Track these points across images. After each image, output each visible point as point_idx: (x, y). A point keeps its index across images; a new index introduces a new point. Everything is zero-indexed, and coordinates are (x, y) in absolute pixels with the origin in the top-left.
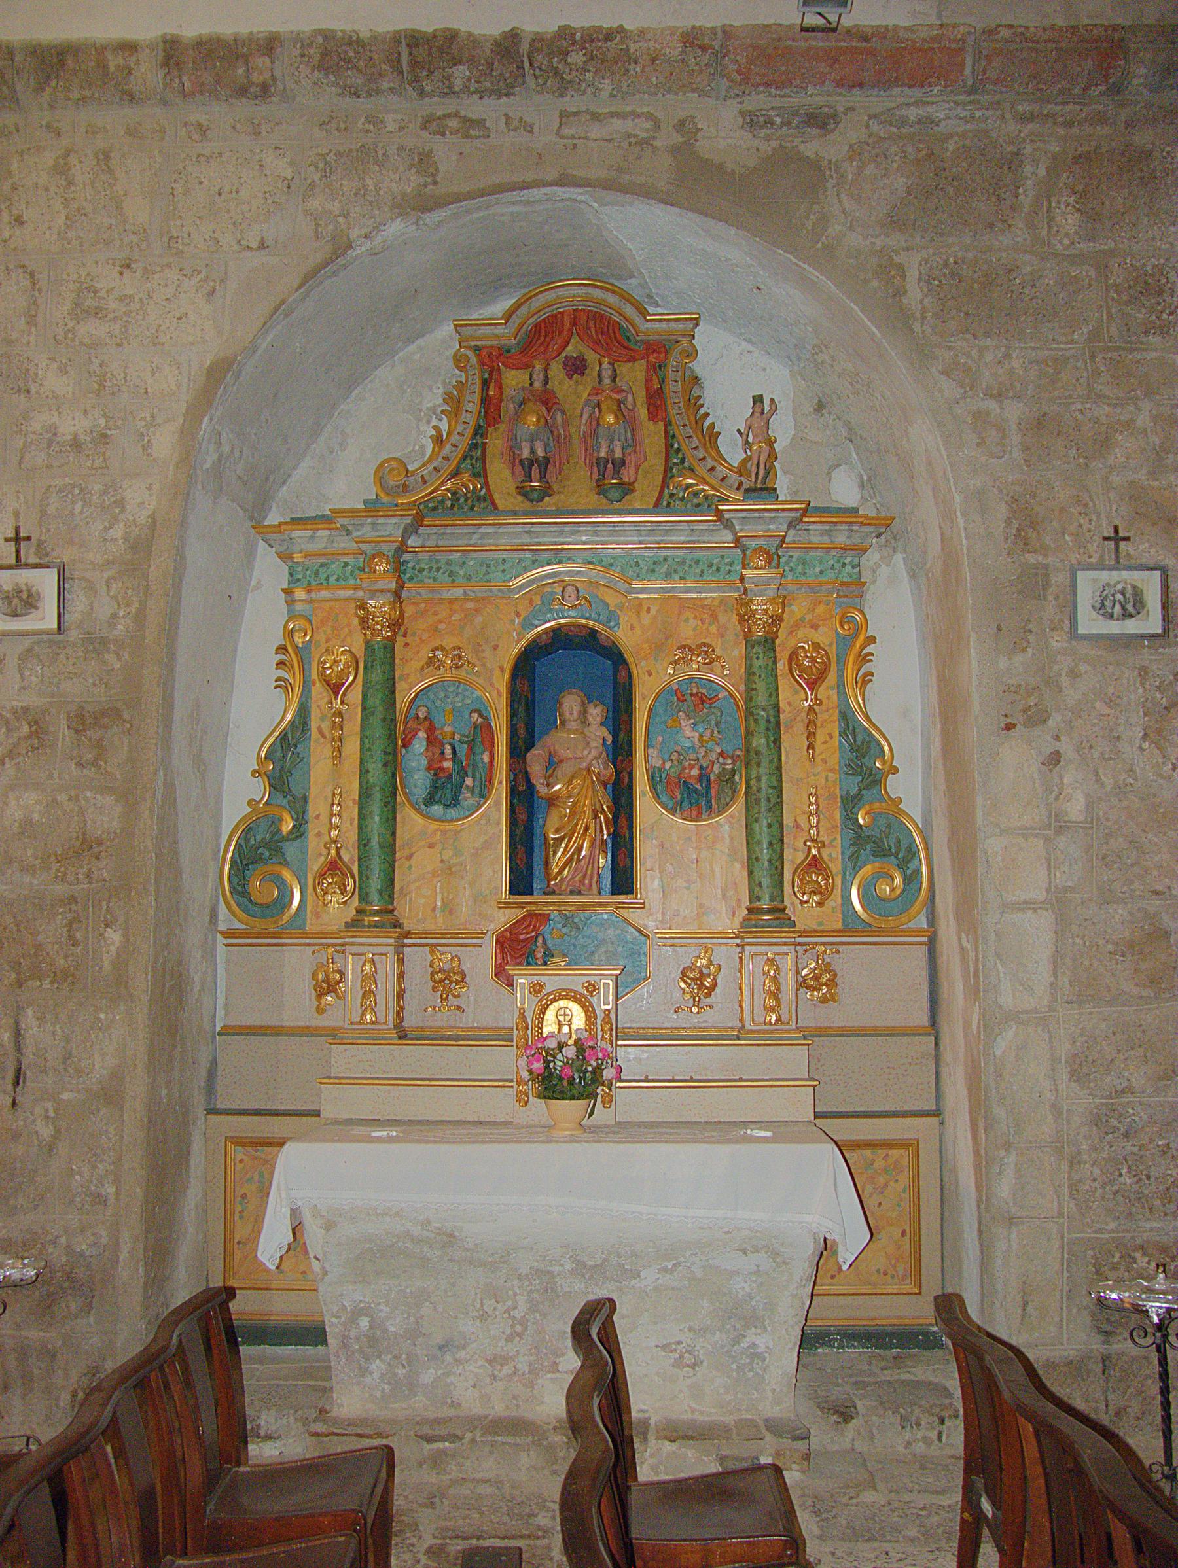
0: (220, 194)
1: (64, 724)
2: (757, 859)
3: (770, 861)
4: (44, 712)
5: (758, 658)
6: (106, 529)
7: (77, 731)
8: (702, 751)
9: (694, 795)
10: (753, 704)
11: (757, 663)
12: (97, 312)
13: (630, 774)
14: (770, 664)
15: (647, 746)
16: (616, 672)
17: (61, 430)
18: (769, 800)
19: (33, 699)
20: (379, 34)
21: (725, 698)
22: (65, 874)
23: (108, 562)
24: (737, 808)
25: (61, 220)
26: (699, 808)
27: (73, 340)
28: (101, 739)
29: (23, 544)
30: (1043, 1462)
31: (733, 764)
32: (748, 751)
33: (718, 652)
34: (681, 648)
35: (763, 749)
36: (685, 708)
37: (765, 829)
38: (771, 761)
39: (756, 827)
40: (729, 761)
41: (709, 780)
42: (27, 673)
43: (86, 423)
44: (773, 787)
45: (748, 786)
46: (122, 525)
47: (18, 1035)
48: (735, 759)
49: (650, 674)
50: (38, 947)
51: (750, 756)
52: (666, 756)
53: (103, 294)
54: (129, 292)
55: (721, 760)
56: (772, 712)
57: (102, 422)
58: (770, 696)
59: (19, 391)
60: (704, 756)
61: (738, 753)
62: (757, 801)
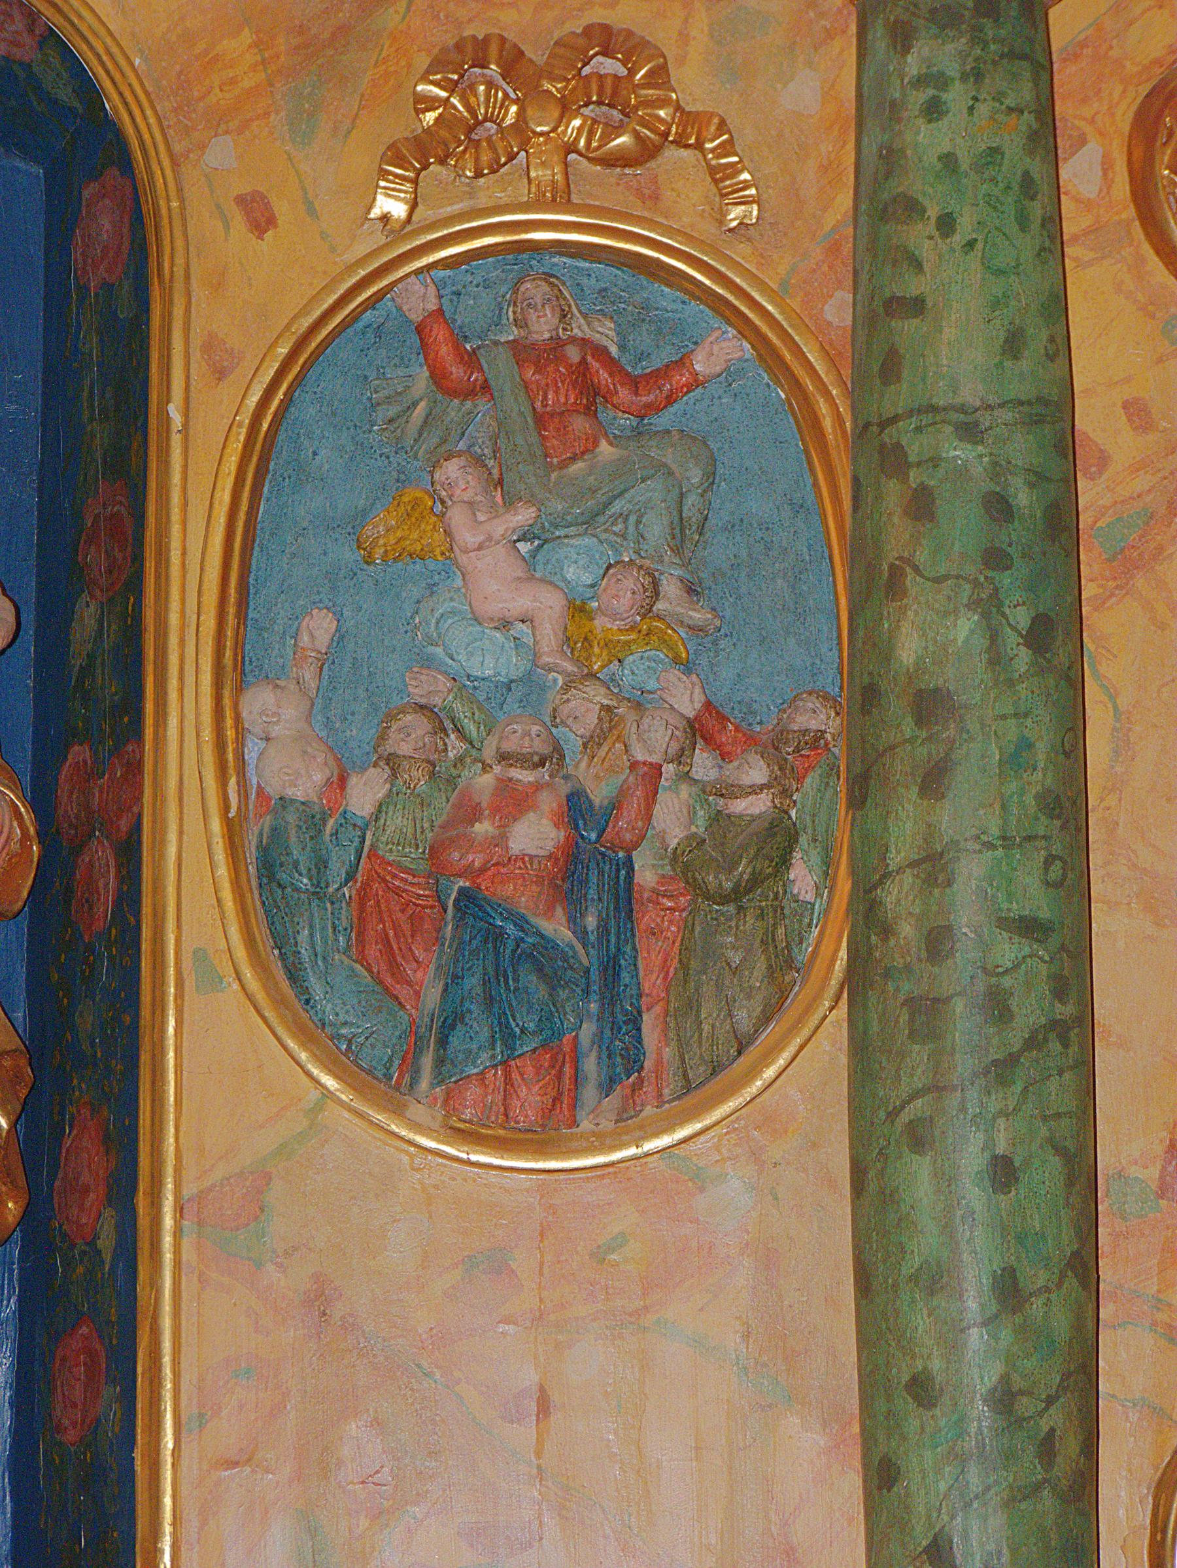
2: (922, 1389)
3: (1004, 1399)
5: (934, 110)
8: (585, 707)
9: (524, 980)
10: (899, 397)
11: (927, 140)
13: (129, 852)
14: (1013, 144)
15: (235, 672)
16: (62, 219)
18: (997, 1006)
20: (1081, 1449)
21: (730, 374)
24: (803, 1070)
26: (560, 1063)
30: (1062, 243)
31: (782, 785)
32: (869, 697)
33: (693, 86)
34: (463, 59)
35: (967, 679)
36: (480, 432)
37: (974, 1194)
38: (1017, 759)
39: (918, 1178)
40: (756, 772)
41: (624, 898)
44: (1028, 927)
45: (869, 917)
48: (791, 754)
49: (260, 218)
51: (881, 729)
52: (360, 734)
55: (704, 764)
56: (1022, 449)
58: (1013, 344)
60: (591, 743)
61: (815, 718)
62: (927, 1013)
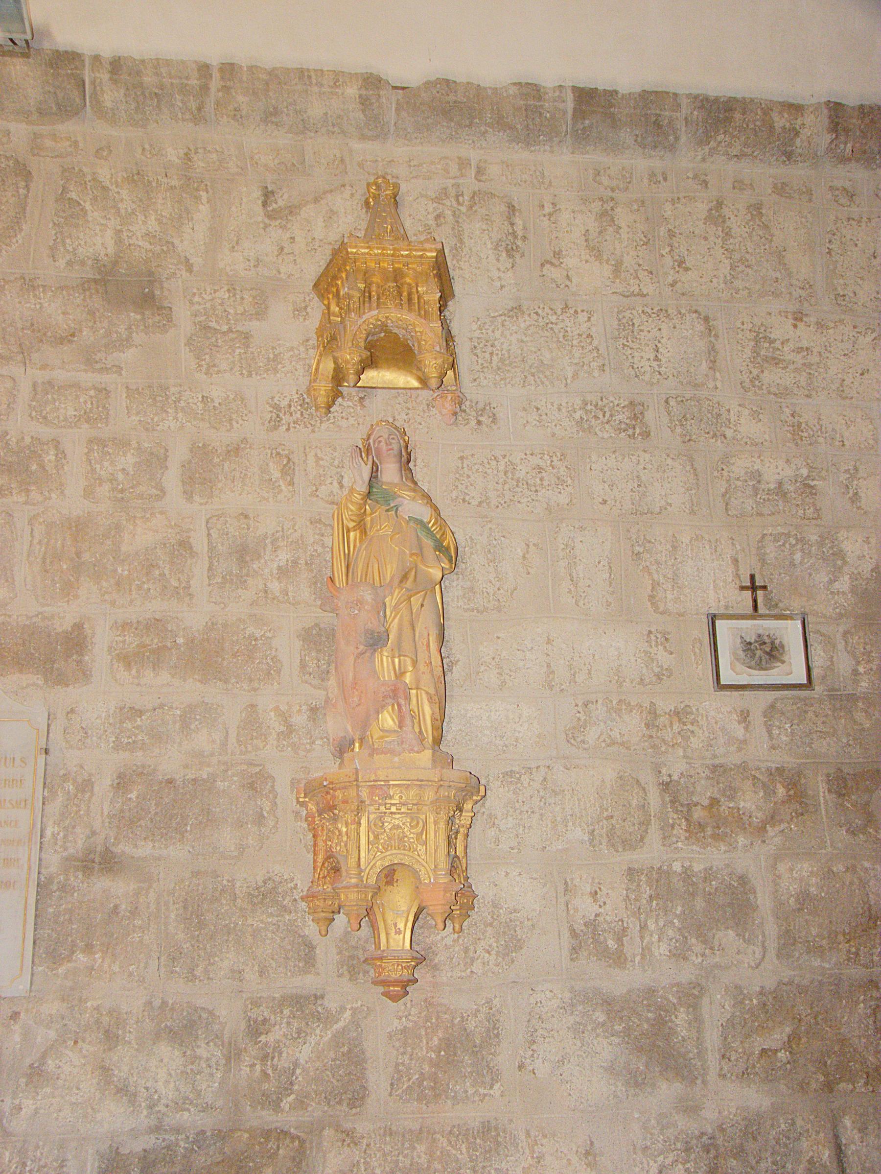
0: (875, 257)
1: (822, 787)
4: (799, 774)
6: (831, 582)
7: (840, 795)
12: (776, 361)
17: (765, 477)
19: (789, 761)
22: (857, 954)
23: (841, 616)
25: (727, 271)
26: (711, 822)
27: (760, 388)
28: (868, 804)
29: (760, 593)
42: (776, 732)
43: (789, 472)
46: (847, 577)
47: (839, 1151)
50: (843, 1041)
53: (777, 344)
54: (805, 344)
57: (804, 472)
59: (715, 435)
